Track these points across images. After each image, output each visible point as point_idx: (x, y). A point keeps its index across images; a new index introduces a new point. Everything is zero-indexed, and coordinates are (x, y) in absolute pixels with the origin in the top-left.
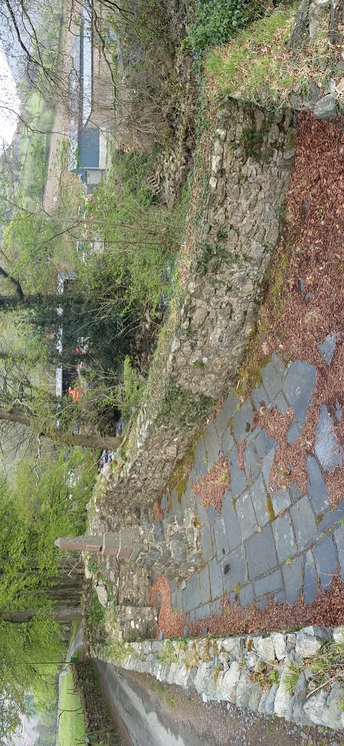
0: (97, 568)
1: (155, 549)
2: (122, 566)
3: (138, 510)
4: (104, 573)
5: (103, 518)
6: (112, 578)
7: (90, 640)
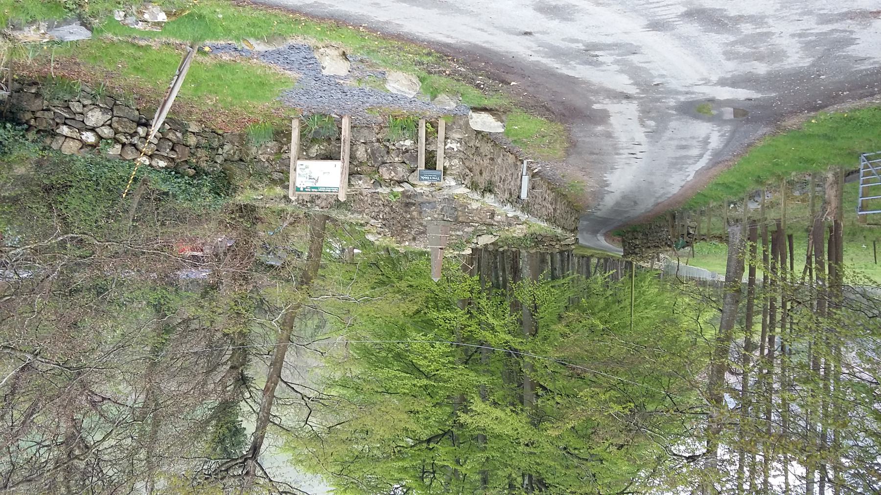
0: (462, 244)
1: (442, 209)
2: (460, 219)
3: (407, 205)
4: (466, 237)
5: (414, 239)
6: (471, 229)
7: (554, 243)
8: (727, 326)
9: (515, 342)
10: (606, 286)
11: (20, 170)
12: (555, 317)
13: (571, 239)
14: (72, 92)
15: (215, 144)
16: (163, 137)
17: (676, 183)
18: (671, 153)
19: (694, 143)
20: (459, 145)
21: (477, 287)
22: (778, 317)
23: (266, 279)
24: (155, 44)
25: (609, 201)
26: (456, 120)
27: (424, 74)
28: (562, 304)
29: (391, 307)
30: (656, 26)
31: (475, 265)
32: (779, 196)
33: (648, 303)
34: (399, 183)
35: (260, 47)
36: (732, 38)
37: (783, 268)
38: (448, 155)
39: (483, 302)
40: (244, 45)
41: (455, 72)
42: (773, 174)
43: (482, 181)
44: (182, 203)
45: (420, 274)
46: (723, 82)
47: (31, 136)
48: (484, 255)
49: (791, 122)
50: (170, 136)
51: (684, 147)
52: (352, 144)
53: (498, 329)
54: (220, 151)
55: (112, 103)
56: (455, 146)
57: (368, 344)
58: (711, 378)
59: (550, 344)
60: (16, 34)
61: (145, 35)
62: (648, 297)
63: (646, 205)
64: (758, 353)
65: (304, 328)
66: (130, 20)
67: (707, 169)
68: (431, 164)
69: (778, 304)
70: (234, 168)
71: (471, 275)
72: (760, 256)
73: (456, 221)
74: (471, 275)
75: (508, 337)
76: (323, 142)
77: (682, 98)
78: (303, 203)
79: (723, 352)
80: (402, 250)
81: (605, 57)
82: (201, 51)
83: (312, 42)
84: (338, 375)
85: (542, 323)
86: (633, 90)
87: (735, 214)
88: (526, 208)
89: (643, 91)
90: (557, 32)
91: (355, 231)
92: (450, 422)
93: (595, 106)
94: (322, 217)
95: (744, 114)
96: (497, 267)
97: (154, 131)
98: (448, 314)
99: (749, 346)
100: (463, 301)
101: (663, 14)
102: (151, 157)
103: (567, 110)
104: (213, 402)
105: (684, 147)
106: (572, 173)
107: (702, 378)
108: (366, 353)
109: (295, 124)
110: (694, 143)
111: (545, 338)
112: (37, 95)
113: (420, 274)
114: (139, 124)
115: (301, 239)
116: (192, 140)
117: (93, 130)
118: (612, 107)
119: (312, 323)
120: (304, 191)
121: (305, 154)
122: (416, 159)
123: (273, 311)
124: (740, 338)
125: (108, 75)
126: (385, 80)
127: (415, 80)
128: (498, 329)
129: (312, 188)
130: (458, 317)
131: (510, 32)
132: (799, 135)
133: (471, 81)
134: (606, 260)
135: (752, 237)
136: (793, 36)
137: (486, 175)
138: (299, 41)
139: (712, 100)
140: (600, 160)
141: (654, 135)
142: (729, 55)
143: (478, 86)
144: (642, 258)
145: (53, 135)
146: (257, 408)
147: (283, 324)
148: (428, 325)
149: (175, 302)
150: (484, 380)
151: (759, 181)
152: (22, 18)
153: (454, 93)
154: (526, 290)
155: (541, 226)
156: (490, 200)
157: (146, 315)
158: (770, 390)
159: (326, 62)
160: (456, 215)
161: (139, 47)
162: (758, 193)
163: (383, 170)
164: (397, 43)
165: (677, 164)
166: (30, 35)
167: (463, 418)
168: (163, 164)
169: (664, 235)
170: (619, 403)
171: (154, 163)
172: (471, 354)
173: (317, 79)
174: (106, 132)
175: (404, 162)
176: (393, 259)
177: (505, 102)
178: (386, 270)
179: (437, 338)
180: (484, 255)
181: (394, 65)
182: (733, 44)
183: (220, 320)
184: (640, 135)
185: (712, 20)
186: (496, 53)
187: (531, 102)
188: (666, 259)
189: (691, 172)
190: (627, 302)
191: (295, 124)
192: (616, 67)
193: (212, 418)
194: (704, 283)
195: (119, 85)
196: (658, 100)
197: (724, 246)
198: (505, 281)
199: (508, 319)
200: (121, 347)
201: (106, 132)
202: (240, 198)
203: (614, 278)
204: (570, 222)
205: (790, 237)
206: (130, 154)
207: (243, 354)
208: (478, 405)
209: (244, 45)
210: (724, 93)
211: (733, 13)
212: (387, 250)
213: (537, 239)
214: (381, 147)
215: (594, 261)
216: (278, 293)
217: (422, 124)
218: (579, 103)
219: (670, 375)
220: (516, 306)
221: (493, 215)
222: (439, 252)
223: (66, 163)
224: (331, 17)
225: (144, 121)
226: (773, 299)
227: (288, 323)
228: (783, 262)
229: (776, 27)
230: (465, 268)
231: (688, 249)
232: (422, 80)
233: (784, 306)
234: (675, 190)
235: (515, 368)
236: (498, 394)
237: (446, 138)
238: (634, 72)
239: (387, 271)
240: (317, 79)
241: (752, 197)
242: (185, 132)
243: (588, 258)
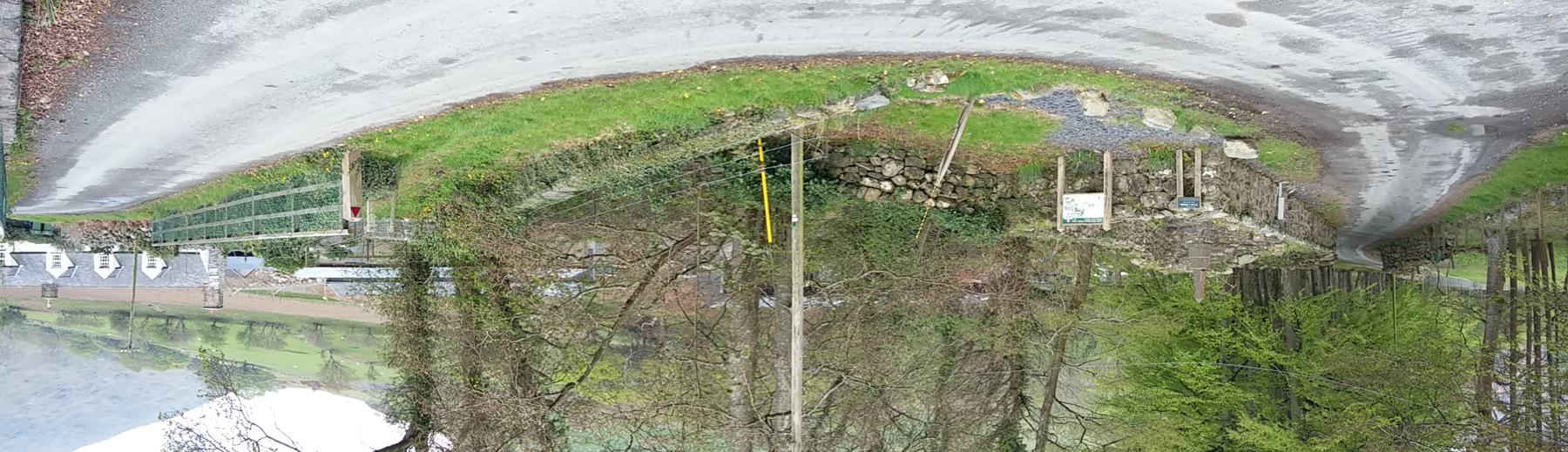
3: (1169, 229)
8: (1491, 337)
9: (1280, 359)
10: (1367, 298)
11: (830, 215)
12: (1318, 332)
13: (1330, 256)
14: (872, 149)
15: (991, 184)
16: (946, 182)
17: (1431, 198)
18: (1424, 169)
19: (1447, 159)
21: (1240, 306)
22: (1544, 325)
23: (1040, 305)
24: (937, 102)
25: (1366, 217)
26: (1210, 149)
27: (1178, 108)
28: (1325, 319)
29: (1157, 328)
30: (1400, 53)
31: (1238, 283)
32: (1535, 207)
33: (1411, 315)
34: (1160, 210)
35: (1029, 96)
36: (1476, 60)
37: (1545, 280)
38: (1206, 182)
39: (1246, 320)
40: (1013, 96)
41: (1208, 105)
42: (1528, 186)
43: (1239, 205)
44: (963, 239)
45: (1184, 295)
46: (1470, 101)
47: (841, 188)
48: (1246, 274)
49: (1542, 135)
50: (952, 180)
51: (1437, 164)
52: (1114, 177)
53: (1262, 347)
55: (903, 154)
56: (1211, 173)
57: (1138, 364)
58: (1478, 389)
59: (1315, 359)
60: (832, 108)
61: (930, 96)
62: (1412, 309)
63: (1402, 220)
64: (1524, 362)
65: (1075, 349)
66: (920, 85)
67: (1460, 183)
68: (1189, 191)
69: (1543, 312)
70: (1008, 205)
71: (1234, 293)
72: (1520, 266)
73: (1217, 242)
74: (1234, 293)
75: (1273, 354)
76: (1087, 177)
77: (1431, 118)
78: (1070, 233)
79: (1489, 363)
80: (1166, 273)
81: (1351, 84)
82: (977, 104)
83: (1074, 87)
84: (1110, 395)
85: (1305, 338)
86: (1382, 113)
87: (1491, 225)
88: (1283, 228)
89: (1392, 113)
90: (1304, 63)
91: (1122, 257)
92: (1219, 438)
93: (1346, 130)
94: (1088, 245)
95: (1495, 129)
96: (1259, 285)
97: (940, 177)
98: (1212, 333)
99: (1515, 356)
100: (1227, 319)
101: (1405, 41)
102: (936, 199)
103: (1316, 133)
104: (997, 418)
105: (1437, 164)
106: (1327, 192)
107: (1469, 390)
108: (1137, 372)
109: (1061, 161)
110: (1447, 159)
111: (1310, 353)
112: (845, 154)
113: (1184, 295)
114: (927, 172)
115: (1069, 266)
116: (970, 182)
117: (889, 179)
118: (1362, 130)
119: (1083, 344)
121: (1071, 188)
123: (1046, 334)
124: (1506, 348)
125: (901, 132)
126: (1142, 116)
127: (1171, 114)
128: (1262, 347)
130: (1223, 335)
131: (1259, 66)
132: (1550, 147)
133: (1224, 113)
134: (1367, 274)
135: (1511, 248)
136: (1537, 55)
137: (1243, 199)
138: (1062, 87)
139: (1461, 119)
140: (1354, 179)
141: (1405, 154)
142: (1475, 76)
143: (1231, 117)
144: (1402, 271)
145: (858, 186)
146: (1036, 426)
147: (1055, 347)
148: (1193, 344)
149: (961, 327)
150: (1250, 396)
151: (1514, 193)
152: (836, 94)
153: (1208, 124)
154: (1287, 307)
155: (1300, 244)
156: (1247, 222)
157: (936, 339)
158: (1540, 400)
159: (1088, 104)
160: (1216, 237)
161: (926, 106)
162: (1514, 205)
163: (1144, 199)
164: (1151, 82)
165: (1431, 180)
166: (842, 108)
167: (1232, 434)
168: (946, 205)
169: (1422, 248)
170: (1385, 415)
172: (1237, 370)
173: (1080, 119)
174: (900, 180)
176: (1158, 282)
177: (1257, 130)
178: (1152, 293)
179: (1204, 357)
180: (1246, 274)
181: (1150, 102)
182: (1478, 65)
183: (1000, 344)
184: (1392, 154)
185: (1455, 44)
186: (1246, 86)
187: (1283, 129)
188: (1425, 271)
189: (1445, 186)
190: (1390, 314)
191: (1061, 161)
192: (1363, 93)
193: (996, 434)
194: (1465, 293)
195: (909, 140)
196: (1408, 121)
197: (1483, 260)
198: (1267, 299)
199: (1272, 335)
200: (914, 368)
201: (900, 180)
202: (1013, 232)
203: (1376, 291)
204: (1328, 240)
205: (1550, 245)
206: (920, 198)
207: (1021, 372)
208: (1245, 421)
209: (1013, 96)
210: (1473, 112)
211: (1475, 37)
212: (1152, 272)
213: (1296, 257)
214: (1140, 178)
215: (1354, 274)
216: (1049, 316)
217: (1179, 153)
218: (1330, 127)
219: (1437, 387)
220: (1279, 322)
221: (1252, 236)
222: (1201, 273)
223: (865, 208)
224: (1090, 64)
226: (1536, 309)
227: (1060, 346)
228: (1545, 273)
229: (1519, 48)
230: (1227, 288)
231: (1447, 261)
232: (1177, 114)
233: (1548, 314)
234: (1431, 204)
235: (1281, 383)
236: (1266, 409)
238: (1381, 96)
239: (1155, 293)
240: (1080, 119)
241: (1508, 208)
242: (964, 175)
243: (1349, 272)
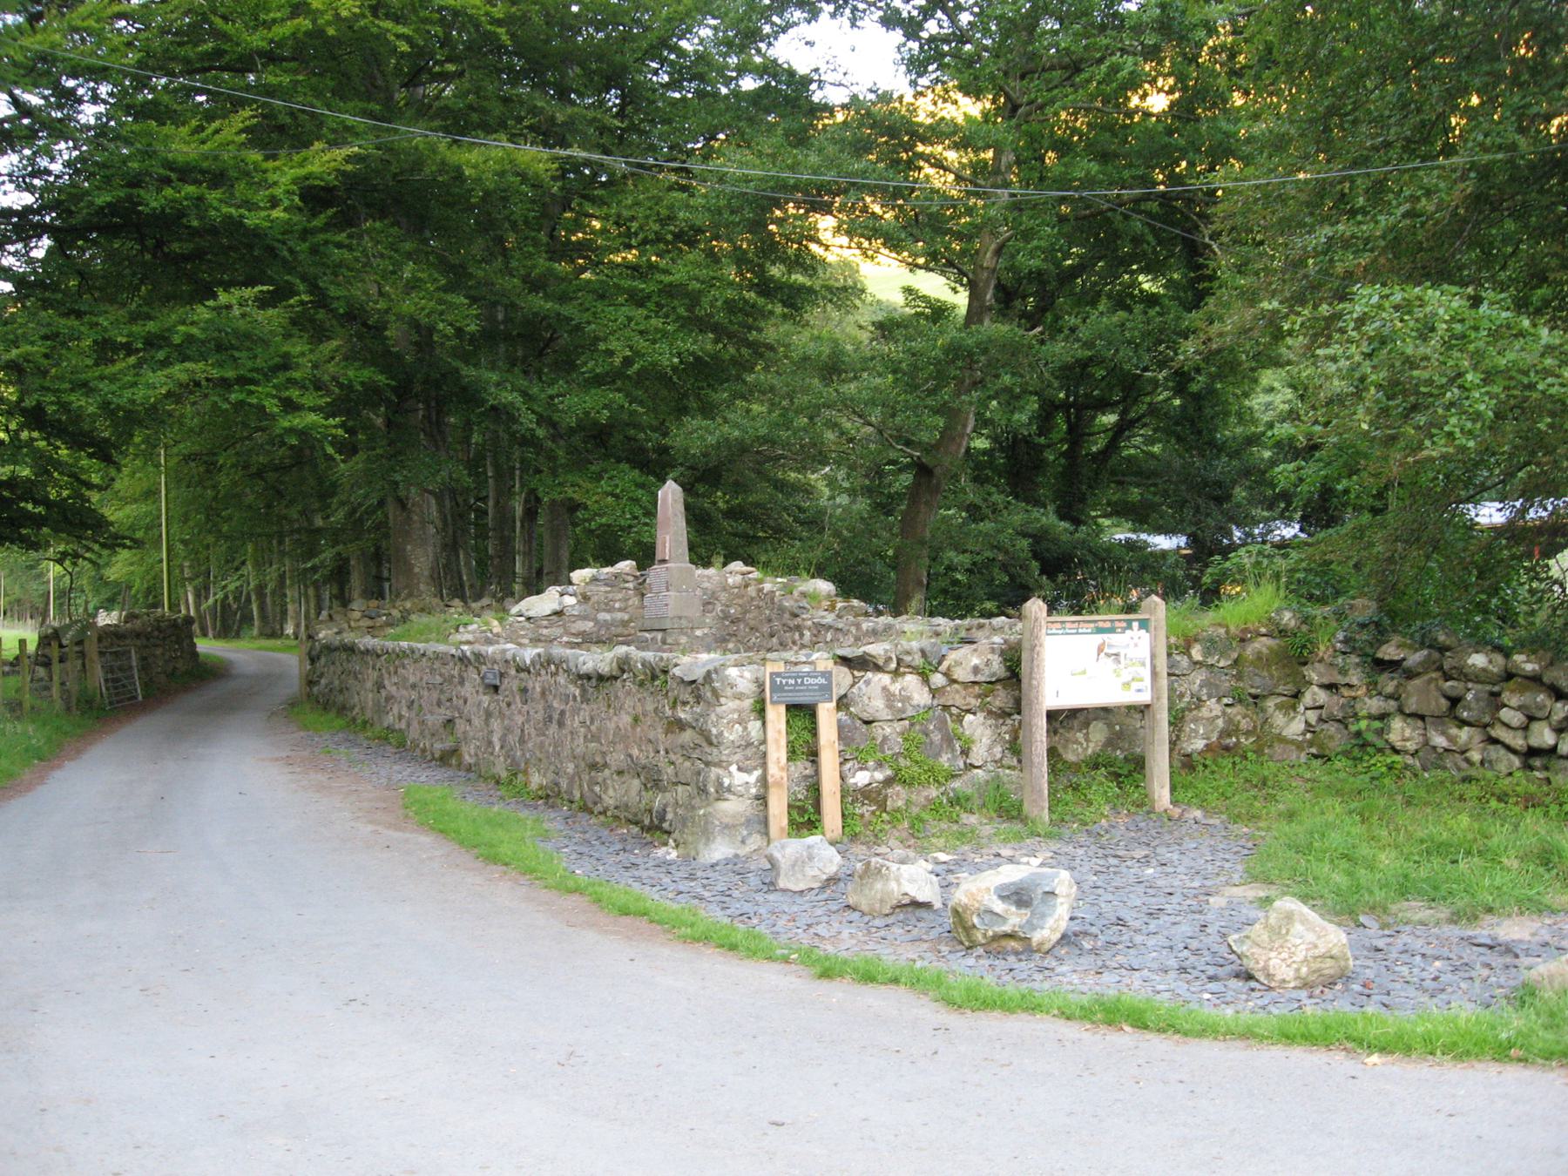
20: (726, 782)
54: (1312, 716)
120: (1129, 622)
122: (843, 733)
129: (1112, 630)
171: (1499, 659)
175: (867, 723)
225: (1537, 762)
237: (762, 799)
